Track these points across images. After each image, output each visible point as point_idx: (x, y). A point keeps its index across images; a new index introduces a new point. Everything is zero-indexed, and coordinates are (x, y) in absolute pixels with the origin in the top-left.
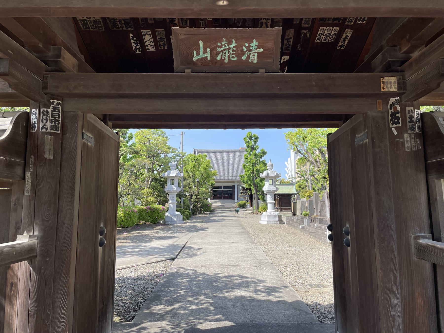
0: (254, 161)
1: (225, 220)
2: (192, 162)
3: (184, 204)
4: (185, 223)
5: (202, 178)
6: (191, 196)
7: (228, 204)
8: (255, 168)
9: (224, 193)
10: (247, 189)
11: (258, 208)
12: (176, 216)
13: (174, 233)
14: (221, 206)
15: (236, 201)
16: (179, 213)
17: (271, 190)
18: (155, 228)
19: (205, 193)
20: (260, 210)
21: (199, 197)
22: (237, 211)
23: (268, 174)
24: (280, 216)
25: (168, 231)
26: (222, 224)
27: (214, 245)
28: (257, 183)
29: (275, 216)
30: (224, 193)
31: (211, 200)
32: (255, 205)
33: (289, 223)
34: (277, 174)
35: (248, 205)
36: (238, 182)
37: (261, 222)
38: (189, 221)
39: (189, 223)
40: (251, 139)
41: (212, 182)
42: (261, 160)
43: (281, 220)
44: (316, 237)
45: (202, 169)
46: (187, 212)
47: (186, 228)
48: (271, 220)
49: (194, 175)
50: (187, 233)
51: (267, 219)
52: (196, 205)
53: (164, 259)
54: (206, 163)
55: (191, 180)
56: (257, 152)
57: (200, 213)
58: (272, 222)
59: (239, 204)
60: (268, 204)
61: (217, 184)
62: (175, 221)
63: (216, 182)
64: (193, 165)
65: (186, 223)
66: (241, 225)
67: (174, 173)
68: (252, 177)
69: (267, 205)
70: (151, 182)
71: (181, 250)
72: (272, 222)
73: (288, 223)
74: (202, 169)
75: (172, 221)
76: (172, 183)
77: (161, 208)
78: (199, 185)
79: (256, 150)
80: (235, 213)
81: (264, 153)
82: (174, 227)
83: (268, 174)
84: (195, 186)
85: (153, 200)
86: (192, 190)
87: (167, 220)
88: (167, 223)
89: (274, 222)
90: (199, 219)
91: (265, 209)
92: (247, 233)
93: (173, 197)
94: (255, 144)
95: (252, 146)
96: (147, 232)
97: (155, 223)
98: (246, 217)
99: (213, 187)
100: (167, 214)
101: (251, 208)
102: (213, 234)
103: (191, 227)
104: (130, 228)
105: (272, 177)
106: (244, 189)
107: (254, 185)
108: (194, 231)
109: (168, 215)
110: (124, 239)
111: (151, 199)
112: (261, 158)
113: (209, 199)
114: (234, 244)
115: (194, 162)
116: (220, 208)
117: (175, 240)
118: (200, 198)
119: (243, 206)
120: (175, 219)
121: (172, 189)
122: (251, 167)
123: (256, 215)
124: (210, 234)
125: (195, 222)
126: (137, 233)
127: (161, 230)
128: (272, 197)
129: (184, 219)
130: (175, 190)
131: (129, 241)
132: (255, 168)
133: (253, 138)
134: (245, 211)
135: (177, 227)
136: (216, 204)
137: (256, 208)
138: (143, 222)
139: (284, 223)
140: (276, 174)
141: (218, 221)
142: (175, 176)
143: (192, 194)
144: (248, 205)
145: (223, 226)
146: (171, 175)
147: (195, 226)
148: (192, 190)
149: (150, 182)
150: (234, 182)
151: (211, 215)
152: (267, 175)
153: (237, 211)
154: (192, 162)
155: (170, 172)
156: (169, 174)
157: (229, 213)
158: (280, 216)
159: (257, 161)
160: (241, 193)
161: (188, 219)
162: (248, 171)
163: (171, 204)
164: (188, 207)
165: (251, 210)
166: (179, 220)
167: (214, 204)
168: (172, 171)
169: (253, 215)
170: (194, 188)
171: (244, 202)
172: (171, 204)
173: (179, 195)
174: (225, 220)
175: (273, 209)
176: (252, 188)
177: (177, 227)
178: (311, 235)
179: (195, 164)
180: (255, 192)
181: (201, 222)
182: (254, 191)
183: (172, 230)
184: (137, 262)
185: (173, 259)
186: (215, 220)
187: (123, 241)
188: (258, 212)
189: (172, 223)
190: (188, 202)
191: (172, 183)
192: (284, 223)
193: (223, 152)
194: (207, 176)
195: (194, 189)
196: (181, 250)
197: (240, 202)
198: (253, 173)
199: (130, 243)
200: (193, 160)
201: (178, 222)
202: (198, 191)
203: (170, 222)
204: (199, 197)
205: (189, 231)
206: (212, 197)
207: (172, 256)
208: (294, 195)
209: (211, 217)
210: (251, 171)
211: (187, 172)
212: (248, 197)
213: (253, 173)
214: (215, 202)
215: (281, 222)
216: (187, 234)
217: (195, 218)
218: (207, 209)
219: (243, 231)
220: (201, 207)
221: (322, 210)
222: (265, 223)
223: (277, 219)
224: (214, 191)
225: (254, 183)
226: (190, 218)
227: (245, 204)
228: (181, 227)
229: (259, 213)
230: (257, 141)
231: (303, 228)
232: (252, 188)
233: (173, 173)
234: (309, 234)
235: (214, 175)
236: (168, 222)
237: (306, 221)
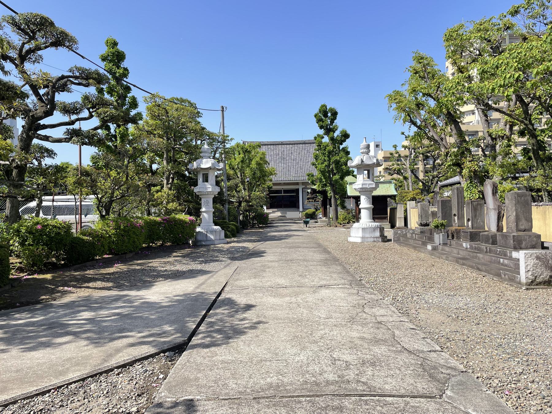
0: (331, 148)
1: (290, 236)
2: (240, 154)
3: (229, 214)
4: (228, 243)
5: (254, 178)
6: (240, 203)
7: (291, 214)
8: (333, 159)
9: (285, 199)
10: (319, 192)
11: (337, 218)
12: (213, 232)
13: (206, 262)
14: (281, 216)
15: (301, 209)
16: (218, 228)
17: (367, 186)
18: (175, 254)
19: (261, 198)
20: (339, 221)
21: (251, 204)
22: (306, 223)
23: (362, 161)
24: (382, 230)
25: (194, 259)
26: (287, 243)
27: (283, 296)
28: (336, 181)
29: (374, 229)
30: (285, 199)
31: (267, 209)
32: (332, 214)
33: (399, 240)
34: (377, 160)
35: (320, 215)
36: (303, 183)
37: (351, 239)
38: (235, 239)
39: (235, 244)
40: (325, 115)
41: (269, 184)
42: (341, 147)
43: (383, 236)
44: (478, 269)
45: (253, 165)
46: (232, 225)
47: (229, 251)
48: (367, 235)
49: (242, 172)
50: (229, 261)
51: (360, 234)
52: (247, 216)
53: (152, 350)
54: (259, 155)
55: (238, 180)
56: (336, 135)
57: (253, 227)
58: (369, 240)
59: (306, 214)
60: (362, 210)
61: (275, 188)
62: (211, 240)
63: (274, 184)
64: (241, 159)
65: (230, 243)
66: (319, 246)
67: (207, 162)
68: (329, 172)
69: (360, 212)
70: (173, 179)
71: (208, 311)
72: (369, 240)
73: (397, 240)
74: (253, 165)
75: (207, 241)
76: (206, 180)
77: (187, 220)
78: (250, 189)
79: (334, 132)
80: (302, 225)
81: (346, 136)
82: (208, 251)
83: (362, 161)
84: (245, 189)
85: (176, 208)
86: (240, 195)
87: (199, 238)
88: (199, 244)
89: (372, 240)
90: (251, 236)
91: (357, 218)
92: (335, 260)
93: (207, 202)
94: (332, 122)
95: (327, 125)
96: (156, 263)
97: (178, 244)
98: (322, 231)
99: (270, 191)
100: (198, 229)
101: (324, 219)
102: (276, 264)
103: (237, 250)
104: (128, 256)
105: (368, 165)
106: (314, 191)
107: (331, 184)
108: (241, 258)
109: (201, 231)
110: (102, 280)
111: (172, 206)
112: (341, 144)
113: (265, 208)
114: (324, 292)
115: (242, 155)
116: (282, 219)
117: (201, 279)
118: (252, 206)
119: (312, 216)
120: (212, 237)
121: (207, 189)
122: (326, 158)
123: (336, 229)
124: (270, 264)
125: (245, 241)
126: (138, 265)
127: (183, 257)
128: (369, 198)
129: (226, 236)
130: (210, 190)
131: (110, 284)
132: (333, 159)
133: (329, 115)
134: (316, 222)
135: (214, 250)
136: (274, 214)
137: (334, 219)
138: (159, 243)
139: (390, 240)
140: (375, 161)
141: (280, 239)
142: (210, 168)
143: (241, 200)
144: (320, 215)
145: (290, 248)
146: (203, 166)
147: (245, 247)
148: (240, 195)
149: (171, 180)
150: (297, 184)
151: (268, 230)
152: (360, 162)
153: (306, 223)
154: (240, 154)
155: (201, 162)
156: (200, 165)
157: (294, 227)
158: (382, 230)
159: (335, 148)
160: (308, 199)
161: (234, 236)
162: (322, 163)
163: (207, 212)
164: (236, 219)
165: (324, 221)
166: (218, 238)
167: (272, 215)
168: (204, 160)
169: (330, 228)
170: (243, 191)
171: (313, 210)
172: (207, 212)
173: (218, 199)
174: (290, 236)
175: (370, 219)
176: (328, 188)
177: (214, 250)
178: (463, 264)
179: (243, 158)
180: (332, 194)
181: (254, 241)
182: (330, 194)
183: (203, 256)
184: (62, 373)
185: (179, 349)
186: (275, 236)
187: (99, 284)
188: (337, 224)
189: (208, 243)
190: (234, 212)
191: (206, 180)
192: (390, 240)
193: (282, 144)
194: (261, 174)
195: (245, 194)
196: (208, 311)
197: (307, 211)
198: (329, 166)
199: (109, 289)
200: (241, 152)
201: (216, 242)
202: (249, 196)
203: (204, 241)
204: (251, 204)
205: (233, 259)
206: (269, 205)
207: (177, 338)
208: (393, 197)
209: (269, 232)
210: (326, 163)
211: (233, 169)
212: (319, 204)
213: (329, 166)
214: (274, 212)
215: (385, 239)
216: (228, 265)
217: (246, 234)
218: (263, 221)
219: (327, 256)
220: (254, 218)
221: (476, 216)
222: (359, 240)
223: (378, 234)
224: (271, 197)
225: (331, 181)
226: (238, 235)
227: (314, 213)
228: (220, 251)
229: (339, 225)
230: (335, 119)
231: (435, 249)
232: (328, 188)
233: (206, 163)
234: (457, 262)
235: (271, 174)
236: (201, 241)
237: (438, 238)
